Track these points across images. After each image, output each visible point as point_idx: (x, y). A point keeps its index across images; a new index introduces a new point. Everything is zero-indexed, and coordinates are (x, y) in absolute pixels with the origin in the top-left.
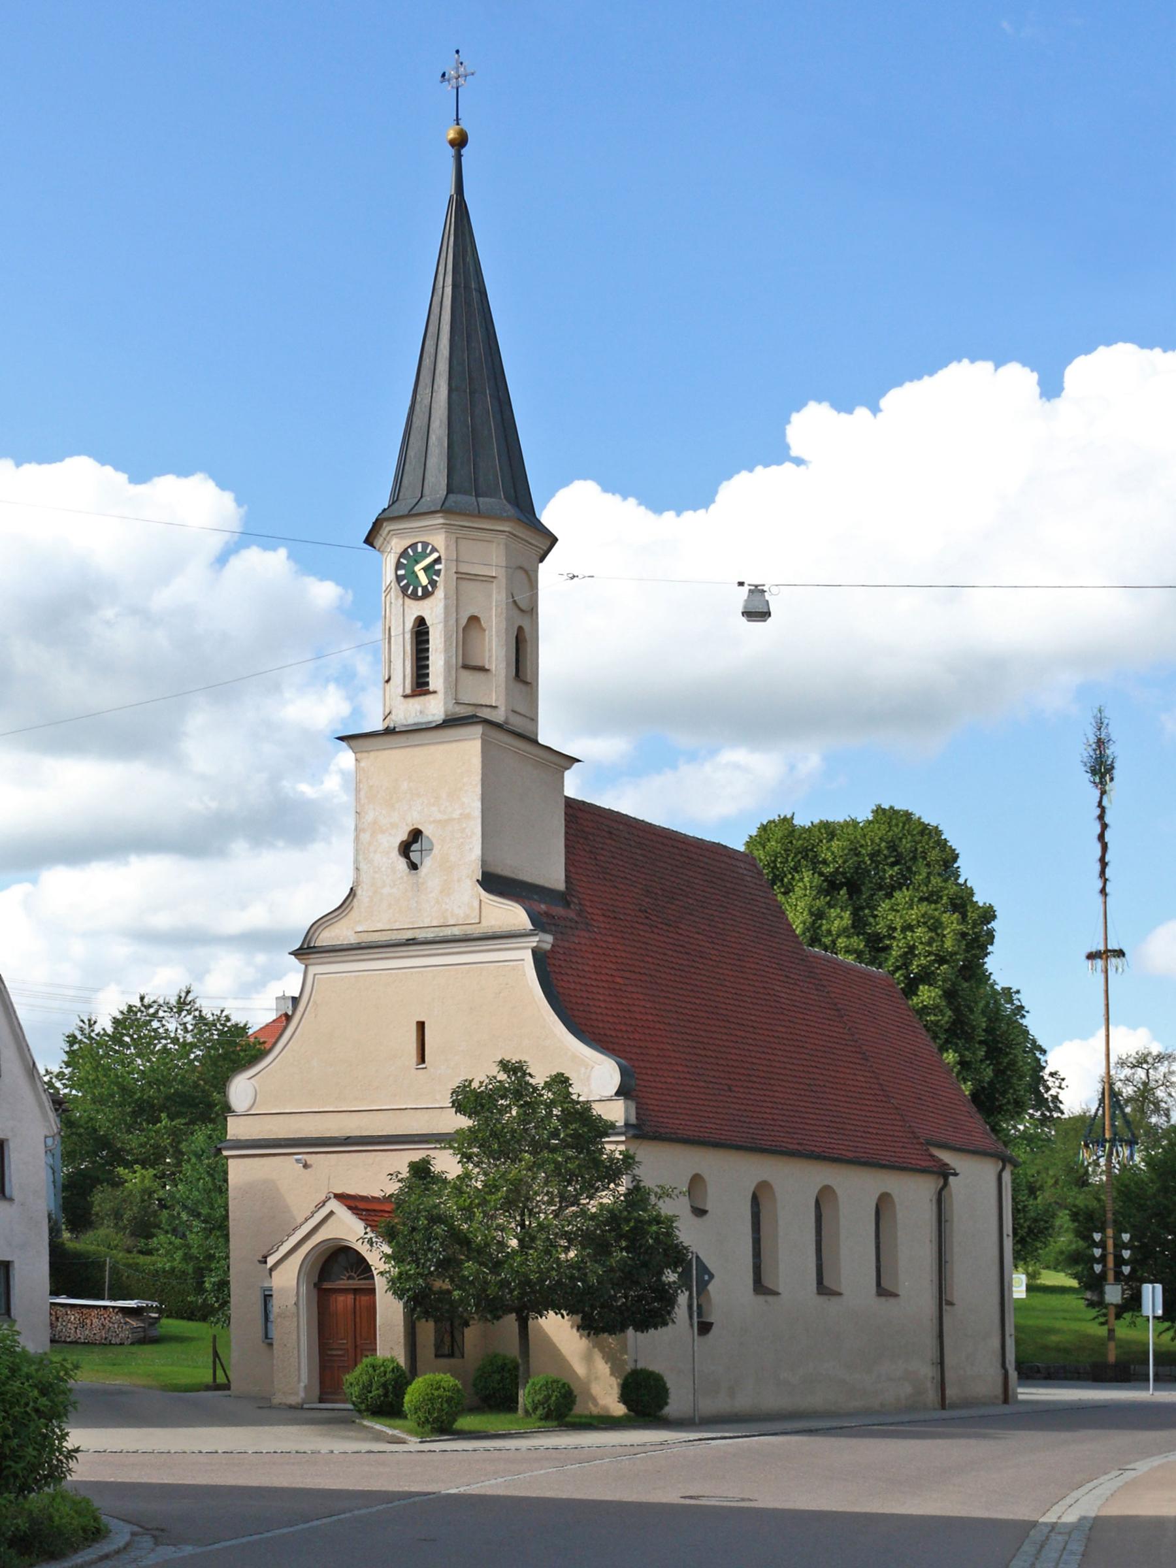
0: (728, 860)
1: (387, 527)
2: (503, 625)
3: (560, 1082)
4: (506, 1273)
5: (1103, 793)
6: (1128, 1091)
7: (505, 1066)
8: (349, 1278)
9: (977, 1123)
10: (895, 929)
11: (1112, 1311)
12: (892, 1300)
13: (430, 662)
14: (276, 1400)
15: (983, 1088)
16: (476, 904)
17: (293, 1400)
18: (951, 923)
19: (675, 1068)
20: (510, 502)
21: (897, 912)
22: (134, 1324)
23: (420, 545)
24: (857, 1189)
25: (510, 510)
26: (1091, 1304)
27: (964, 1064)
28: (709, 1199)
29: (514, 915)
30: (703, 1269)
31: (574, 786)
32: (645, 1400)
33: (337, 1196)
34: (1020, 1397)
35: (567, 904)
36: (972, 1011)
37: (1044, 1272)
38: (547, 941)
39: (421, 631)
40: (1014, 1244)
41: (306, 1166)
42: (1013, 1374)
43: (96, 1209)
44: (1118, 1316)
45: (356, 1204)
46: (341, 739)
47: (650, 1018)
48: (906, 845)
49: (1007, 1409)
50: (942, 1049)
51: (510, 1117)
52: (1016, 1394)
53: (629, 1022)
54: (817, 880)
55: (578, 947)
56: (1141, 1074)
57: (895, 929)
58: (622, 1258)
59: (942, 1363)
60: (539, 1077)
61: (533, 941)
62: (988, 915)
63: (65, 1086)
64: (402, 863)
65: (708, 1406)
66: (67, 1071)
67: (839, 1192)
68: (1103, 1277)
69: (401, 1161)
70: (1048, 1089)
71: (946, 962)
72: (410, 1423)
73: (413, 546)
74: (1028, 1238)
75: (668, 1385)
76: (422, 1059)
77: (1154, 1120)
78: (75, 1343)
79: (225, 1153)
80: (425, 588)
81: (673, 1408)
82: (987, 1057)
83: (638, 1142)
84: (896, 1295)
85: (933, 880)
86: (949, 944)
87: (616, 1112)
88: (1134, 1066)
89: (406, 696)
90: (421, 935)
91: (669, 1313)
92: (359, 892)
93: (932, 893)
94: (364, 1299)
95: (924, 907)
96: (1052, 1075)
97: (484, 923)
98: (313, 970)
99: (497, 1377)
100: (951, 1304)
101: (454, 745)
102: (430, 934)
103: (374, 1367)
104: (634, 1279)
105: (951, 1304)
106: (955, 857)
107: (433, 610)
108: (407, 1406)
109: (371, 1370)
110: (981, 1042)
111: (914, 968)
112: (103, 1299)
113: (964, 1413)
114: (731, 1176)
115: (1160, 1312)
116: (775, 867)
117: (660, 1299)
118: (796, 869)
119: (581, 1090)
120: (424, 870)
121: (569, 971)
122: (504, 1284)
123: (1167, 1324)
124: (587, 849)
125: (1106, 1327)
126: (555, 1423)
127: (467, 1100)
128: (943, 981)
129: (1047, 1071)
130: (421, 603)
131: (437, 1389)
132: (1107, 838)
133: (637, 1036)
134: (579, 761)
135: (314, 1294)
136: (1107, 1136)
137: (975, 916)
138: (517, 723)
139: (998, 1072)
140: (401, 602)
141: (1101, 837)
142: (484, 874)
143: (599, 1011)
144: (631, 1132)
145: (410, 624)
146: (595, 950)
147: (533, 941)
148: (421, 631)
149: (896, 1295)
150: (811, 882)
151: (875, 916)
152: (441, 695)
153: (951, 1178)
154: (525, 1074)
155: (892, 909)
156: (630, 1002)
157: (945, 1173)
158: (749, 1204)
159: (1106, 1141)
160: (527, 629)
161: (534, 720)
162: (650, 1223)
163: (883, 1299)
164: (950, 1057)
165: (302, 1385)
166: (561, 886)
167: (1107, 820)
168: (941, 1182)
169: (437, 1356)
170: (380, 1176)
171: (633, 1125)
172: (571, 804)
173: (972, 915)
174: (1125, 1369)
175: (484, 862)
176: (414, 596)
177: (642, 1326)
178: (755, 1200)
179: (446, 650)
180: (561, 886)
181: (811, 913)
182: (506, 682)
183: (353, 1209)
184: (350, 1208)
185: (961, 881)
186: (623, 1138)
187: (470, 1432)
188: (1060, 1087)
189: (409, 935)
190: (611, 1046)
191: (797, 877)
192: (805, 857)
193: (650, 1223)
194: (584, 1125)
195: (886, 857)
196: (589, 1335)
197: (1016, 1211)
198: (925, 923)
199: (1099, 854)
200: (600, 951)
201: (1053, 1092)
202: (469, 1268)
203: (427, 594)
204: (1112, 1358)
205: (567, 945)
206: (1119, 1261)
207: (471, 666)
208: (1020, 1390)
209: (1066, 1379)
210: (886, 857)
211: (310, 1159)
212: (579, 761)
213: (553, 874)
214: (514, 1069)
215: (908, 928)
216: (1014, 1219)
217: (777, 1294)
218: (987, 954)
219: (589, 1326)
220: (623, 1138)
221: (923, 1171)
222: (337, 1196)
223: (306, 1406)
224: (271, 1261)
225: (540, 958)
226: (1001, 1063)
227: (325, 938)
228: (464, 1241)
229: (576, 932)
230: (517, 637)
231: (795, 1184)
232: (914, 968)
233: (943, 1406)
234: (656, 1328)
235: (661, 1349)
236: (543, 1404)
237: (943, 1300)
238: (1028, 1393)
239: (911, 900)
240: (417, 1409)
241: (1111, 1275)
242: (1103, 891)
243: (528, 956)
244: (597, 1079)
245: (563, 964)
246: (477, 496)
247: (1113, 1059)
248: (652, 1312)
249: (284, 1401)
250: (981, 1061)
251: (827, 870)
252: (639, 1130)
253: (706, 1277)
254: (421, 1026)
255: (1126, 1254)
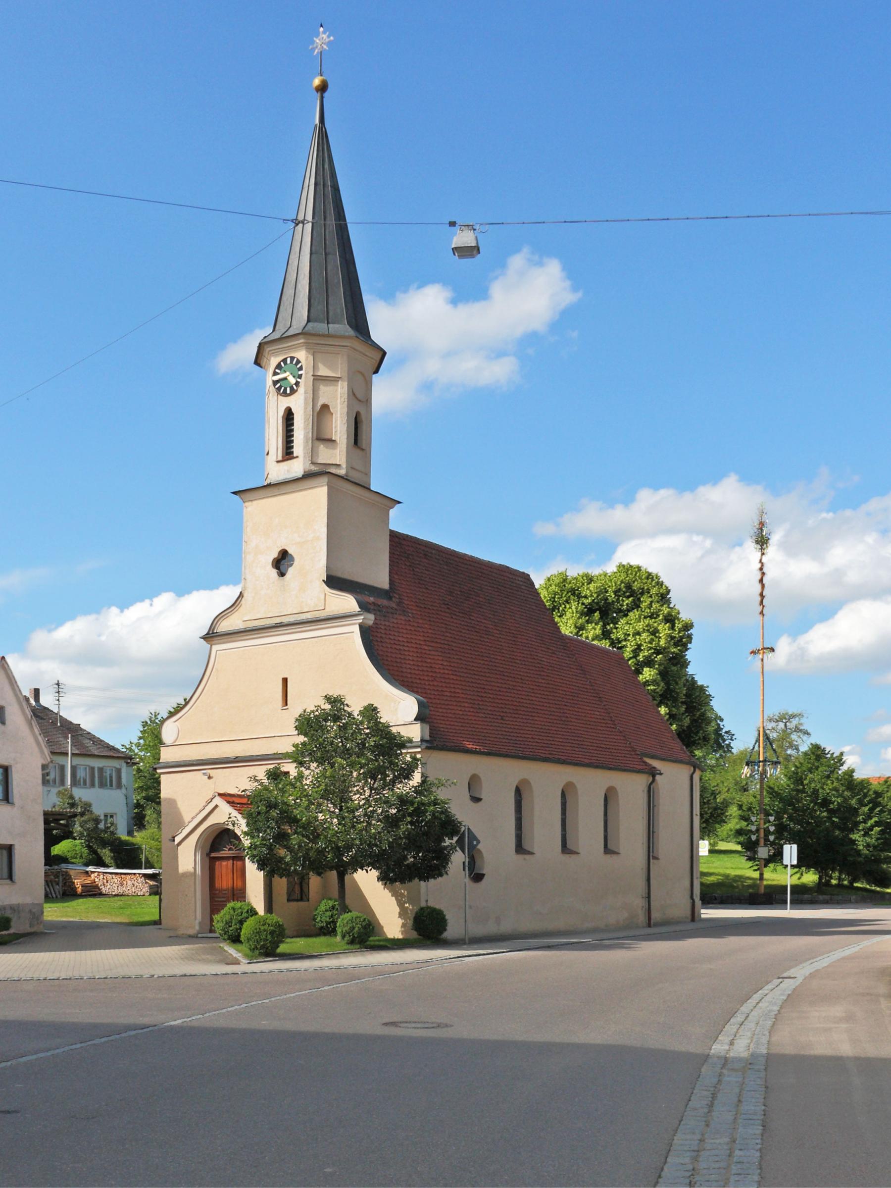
0: (511, 576)
1: (268, 349)
2: (345, 410)
3: (371, 712)
4: (331, 841)
5: (763, 554)
6: (773, 735)
7: (328, 699)
8: (230, 849)
9: (678, 745)
10: (629, 635)
11: (763, 862)
12: (615, 856)
13: (294, 438)
14: (180, 932)
15: (684, 730)
16: (322, 597)
17: (192, 932)
18: (664, 630)
19: (463, 704)
20: (351, 327)
21: (630, 627)
22: (151, 883)
23: (289, 360)
24: (591, 783)
25: (351, 332)
26: (750, 859)
27: (672, 716)
28: (479, 792)
29: (348, 603)
30: (472, 837)
31: (400, 522)
32: (428, 928)
33: (220, 795)
34: (703, 916)
35: (390, 598)
36: (677, 683)
37: (720, 843)
38: (370, 619)
39: (289, 416)
40: (701, 824)
41: (210, 778)
42: (698, 902)
43: (147, 818)
44: (766, 866)
45: (229, 798)
46: (234, 493)
47: (446, 672)
48: (636, 586)
49: (691, 926)
50: (659, 705)
51: (329, 732)
52: (700, 914)
53: (430, 674)
54: (580, 607)
55: (396, 626)
56: (781, 725)
57: (629, 635)
58: (407, 829)
59: (649, 897)
60: (355, 707)
61: (360, 619)
62: (688, 626)
63: (141, 751)
64: (274, 572)
65: (477, 930)
66: (142, 741)
67: (578, 786)
68: (756, 843)
69: (261, 771)
70: (724, 740)
71: (661, 653)
72: (244, 947)
73: (285, 361)
74: (711, 818)
75: (447, 917)
76: (285, 702)
77: (789, 752)
78: (117, 895)
79: (158, 771)
80: (292, 388)
81: (450, 933)
82: (686, 711)
83: (430, 752)
84: (618, 853)
85: (654, 606)
86: (662, 643)
87: (415, 732)
88: (778, 721)
89: (278, 462)
90: (285, 620)
91: (445, 867)
92: (245, 595)
93: (652, 614)
94: (239, 863)
95: (647, 621)
96: (726, 732)
97: (327, 609)
98: (215, 648)
99: (329, 914)
100: (656, 858)
101: (309, 491)
102: (291, 619)
103: (234, 909)
104: (419, 846)
105: (656, 858)
106: (668, 592)
107: (298, 403)
108: (242, 938)
109: (232, 912)
110: (682, 703)
111: (641, 658)
112: (141, 868)
113: (664, 929)
114: (501, 775)
115: (795, 862)
116: (554, 601)
117: (437, 858)
118: (567, 601)
119: (385, 717)
120: (288, 576)
121: (388, 641)
122: (321, 852)
123: (796, 870)
124: (408, 564)
125: (758, 872)
126: (358, 946)
127: (308, 725)
128: (659, 665)
129: (724, 731)
130: (289, 398)
131: (263, 925)
132: (765, 581)
133: (436, 684)
134: (399, 502)
135: (208, 860)
136: (761, 759)
137: (680, 626)
138: (355, 476)
139: (693, 721)
140: (275, 398)
141: (761, 581)
142: (328, 576)
143: (408, 666)
144: (425, 745)
145: (281, 413)
146: (408, 628)
147: (360, 619)
148: (289, 416)
149: (618, 853)
150: (576, 608)
151: (616, 628)
152: (301, 459)
153: (658, 777)
154: (343, 703)
155: (627, 623)
156: (433, 661)
157: (653, 773)
158: (513, 794)
159: (760, 762)
160: (363, 412)
161: (367, 474)
162: (429, 804)
163: (608, 856)
164: (663, 710)
165: (197, 921)
166: (386, 586)
167: (765, 570)
168: (651, 779)
169: (288, 900)
170: (241, 781)
171: (427, 741)
172: (392, 532)
173: (678, 625)
174: (772, 896)
175: (328, 568)
176: (285, 394)
177: (425, 878)
178: (518, 792)
179: (305, 428)
180: (386, 586)
181: (576, 627)
182: (347, 447)
183: (231, 803)
184: (228, 802)
185: (671, 606)
186: (419, 750)
187: (290, 955)
188: (731, 739)
189: (278, 620)
190: (415, 690)
191: (568, 606)
192: (574, 594)
193: (429, 804)
194: (389, 743)
195: (625, 593)
196: (385, 884)
197: (702, 804)
198: (648, 630)
199: (759, 590)
200: (413, 629)
201: (727, 742)
202: (295, 840)
203: (293, 391)
204: (762, 890)
205: (387, 623)
206: (767, 832)
207: (320, 437)
208: (703, 911)
209: (732, 903)
210: (625, 593)
211: (212, 773)
212: (399, 502)
213: (382, 580)
214: (335, 701)
215: (638, 633)
216: (701, 808)
217: (533, 853)
218: (687, 649)
219: (384, 878)
220: (419, 750)
221: (639, 772)
222: (220, 795)
223: (200, 935)
224: (178, 840)
225: (365, 632)
226: (694, 715)
227: (224, 626)
228: (294, 821)
229: (396, 616)
230: (356, 418)
231: (546, 780)
232: (641, 658)
233: (649, 925)
234: (435, 878)
235: (445, 891)
236: (349, 933)
237: (651, 854)
238: (708, 913)
239: (640, 617)
240: (249, 940)
241: (762, 842)
242: (762, 613)
243: (356, 629)
244: (400, 711)
245: (384, 636)
246: (328, 323)
247: (766, 717)
248: (434, 866)
249: (185, 932)
250: (683, 714)
251: (586, 601)
252: (433, 743)
253: (475, 843)
254: (285, 681)
255: (772, 829)
